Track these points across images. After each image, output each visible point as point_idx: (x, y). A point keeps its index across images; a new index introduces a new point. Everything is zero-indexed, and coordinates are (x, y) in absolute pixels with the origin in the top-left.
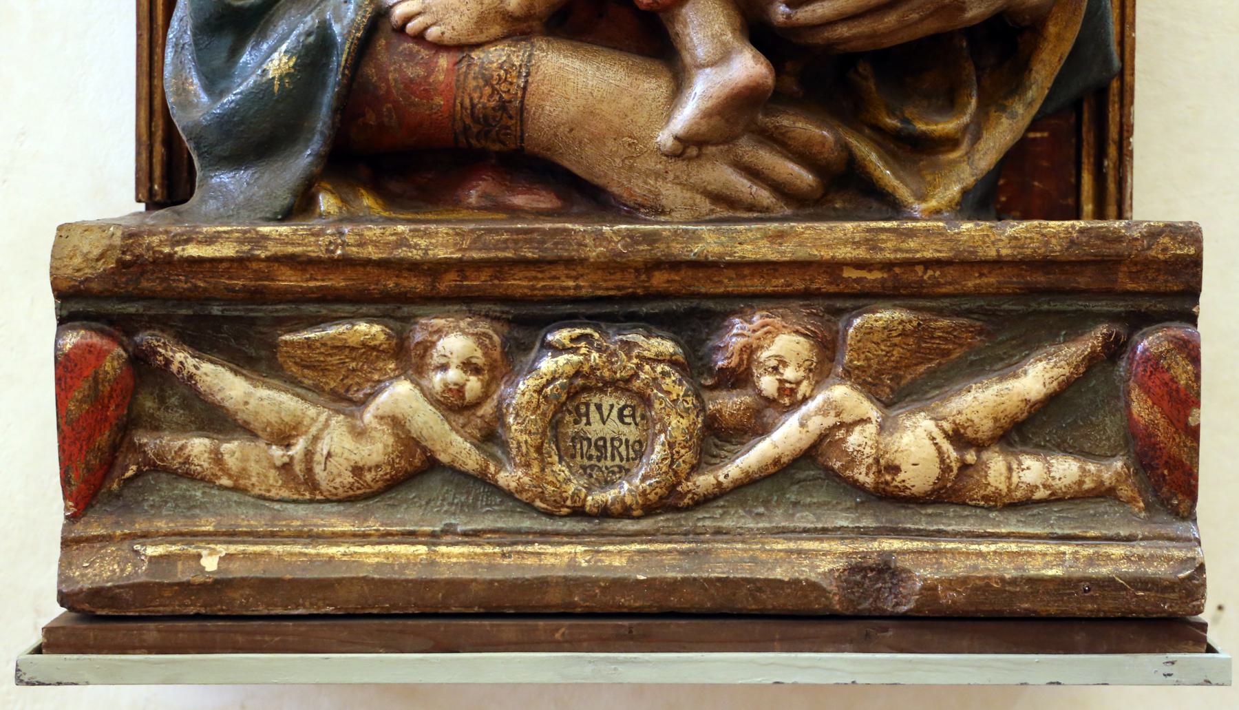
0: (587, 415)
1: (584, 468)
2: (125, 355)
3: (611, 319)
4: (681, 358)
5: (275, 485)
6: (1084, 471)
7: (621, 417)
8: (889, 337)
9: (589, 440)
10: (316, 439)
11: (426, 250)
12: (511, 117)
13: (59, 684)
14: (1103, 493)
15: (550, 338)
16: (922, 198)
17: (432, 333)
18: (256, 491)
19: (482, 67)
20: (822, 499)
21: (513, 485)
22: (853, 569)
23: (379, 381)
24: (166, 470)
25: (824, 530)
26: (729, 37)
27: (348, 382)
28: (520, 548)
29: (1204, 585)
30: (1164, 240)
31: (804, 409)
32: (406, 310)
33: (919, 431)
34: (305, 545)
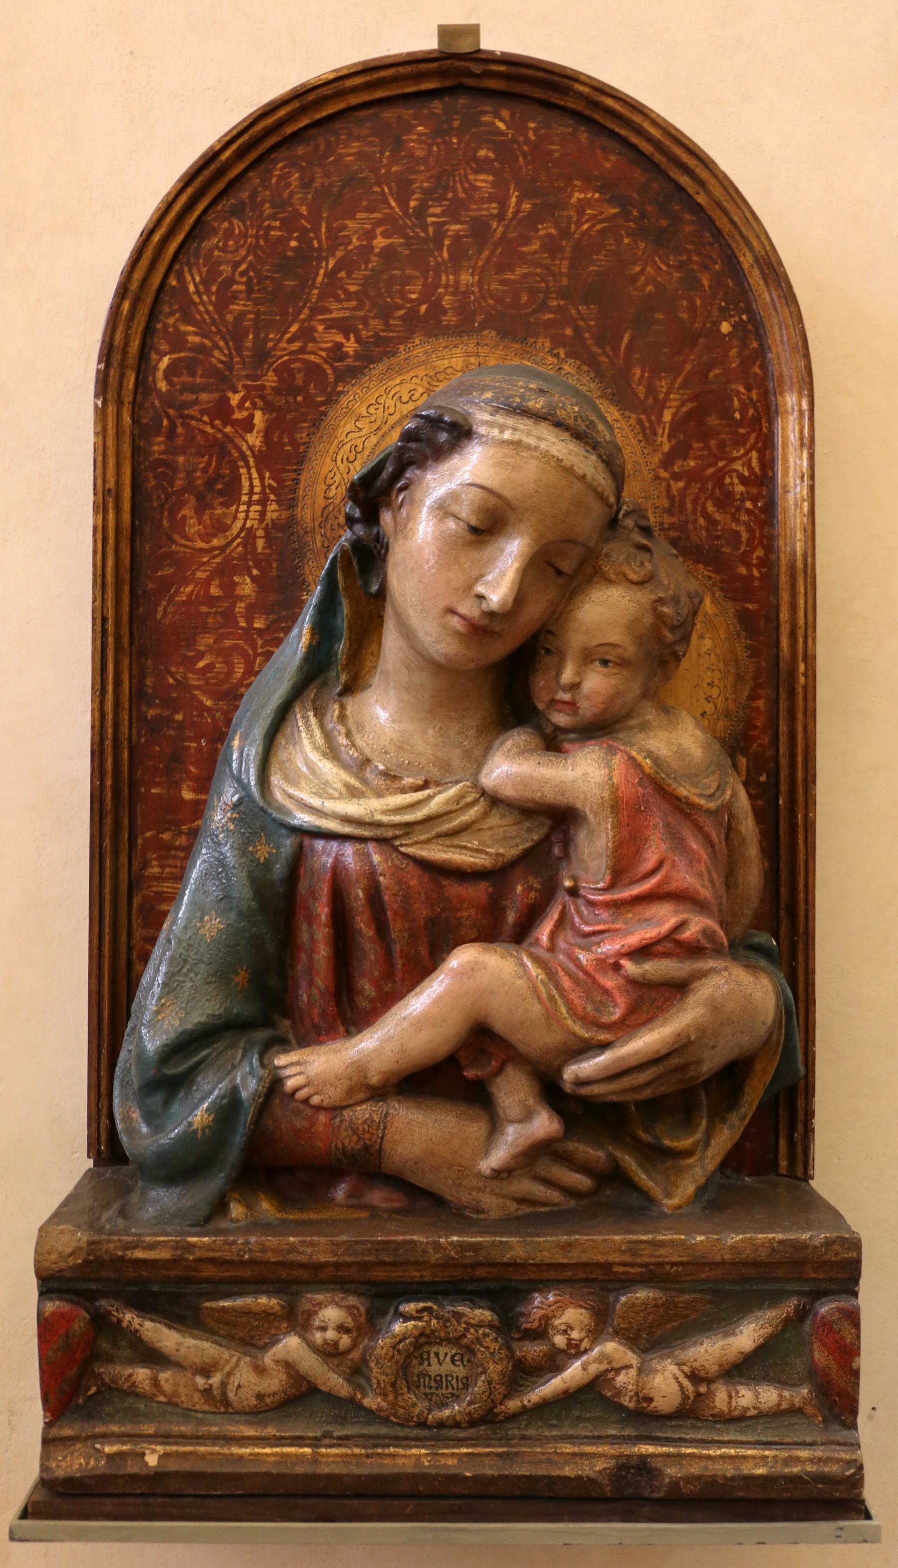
0: (428, 1359)
1: (426, 1395)
2: (87, 1316)
3: (445, 1293)
4: (497, 1323)
5: (200, 1404)
6: (780, 1396)
7: (453, 1361)
8: (645, 1309)
9: (430, 1376)
10: (229, 1374)
11: (311, 1256)
12: (372, 1155)
13: (41, 1541)
14: (795, 1411)
15: (401, 1308)
16: (669, 1195)
17: (314, 1306)
18: (185, 1405)
19: (351, 1122)
20: (599, 1414)
21: (374, 1407)
22: (620, 1467)
23: (275, 1335)
24: (117, 1389)
25: (599, 1437)
26: (531, 1101)
27: (253, 1333)
28: (379, 1450)
29: (862, 1478)
30: (836, 1247)
31: (585, 1358)
32: (295, 1288)
33: (667, 1373)
34: (222, 1446)
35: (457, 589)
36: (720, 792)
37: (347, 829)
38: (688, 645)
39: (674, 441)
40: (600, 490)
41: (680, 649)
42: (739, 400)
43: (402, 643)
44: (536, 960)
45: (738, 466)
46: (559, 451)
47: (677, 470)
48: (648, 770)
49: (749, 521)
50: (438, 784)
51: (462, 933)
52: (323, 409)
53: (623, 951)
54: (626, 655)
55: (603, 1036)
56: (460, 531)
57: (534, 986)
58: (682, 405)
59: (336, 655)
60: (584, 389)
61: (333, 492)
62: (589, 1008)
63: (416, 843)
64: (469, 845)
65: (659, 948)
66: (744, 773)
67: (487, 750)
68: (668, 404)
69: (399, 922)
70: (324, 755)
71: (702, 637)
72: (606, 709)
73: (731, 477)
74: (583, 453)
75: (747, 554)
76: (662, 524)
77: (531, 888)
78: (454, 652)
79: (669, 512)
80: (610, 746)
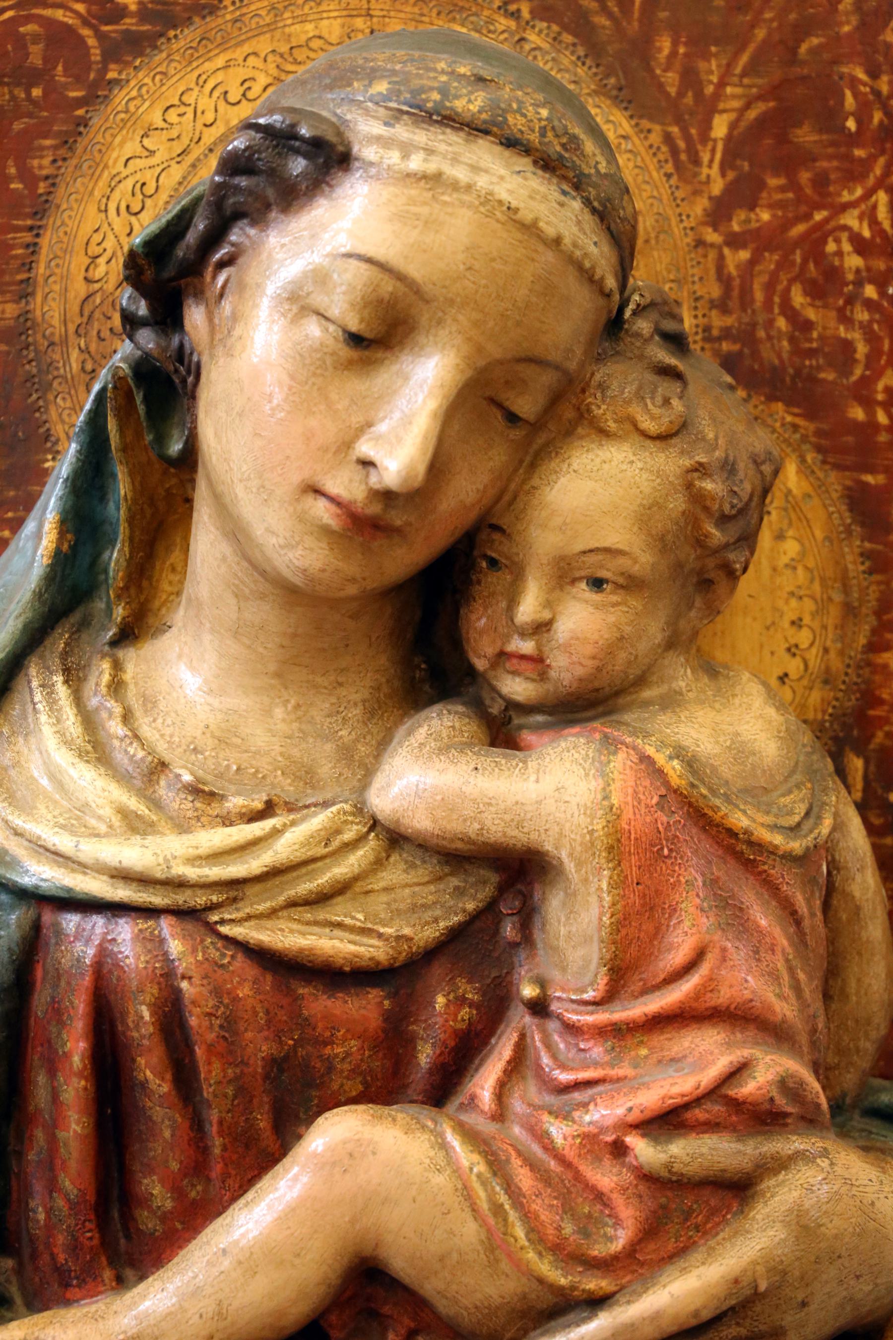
35: (324, 449)
36: (811, 821)
37: (122, 893)
38: (752, 553)
39: (731, 175)
40: (587, 265)
41: (736, 558)
42: (855, 95)
43: (225, 548)
44: (471, 1136)
45: (851, 220)
46: (511, 192)
47: (736, 227)
48: (675, 781)
49: (871, 322)
50: (291, 808)
51: (335, 1086)
52: (80, 112)
53: (630, 1118)
54: (636, 569)
55: (594, 1284)
56: (330, 342)
57: (465, 1187)
58: (748, 106)
59: (106, 571)
60: (564, 78)
61: (99, 272)
62: (568, 1229)
63: (249, 918)
64: (348, 921)
65: (699, 1114)
66: (859, 785)
67: (383, 745)
68: (721, 106)
69: (217, 1065)
70: (81, 754)
71: (780, 537)
72: (599, 669)
73: (838, 241)
74: (557, 196)
75: (866, 382)
76: (707, 329)
77: (462, 1001)
78: (318, 565)
79: (722, 306)
80: (606, 736)
